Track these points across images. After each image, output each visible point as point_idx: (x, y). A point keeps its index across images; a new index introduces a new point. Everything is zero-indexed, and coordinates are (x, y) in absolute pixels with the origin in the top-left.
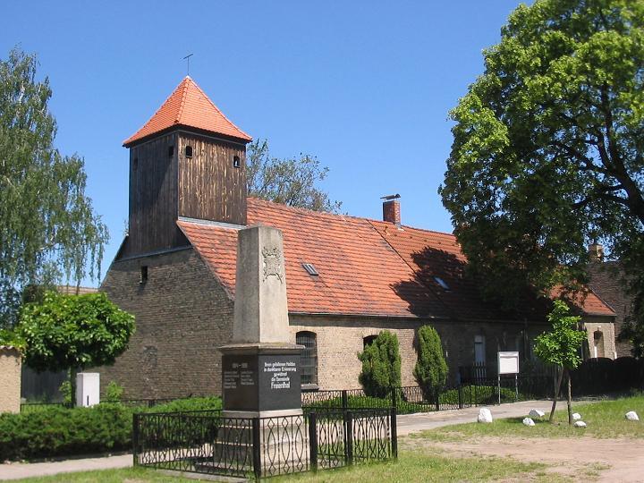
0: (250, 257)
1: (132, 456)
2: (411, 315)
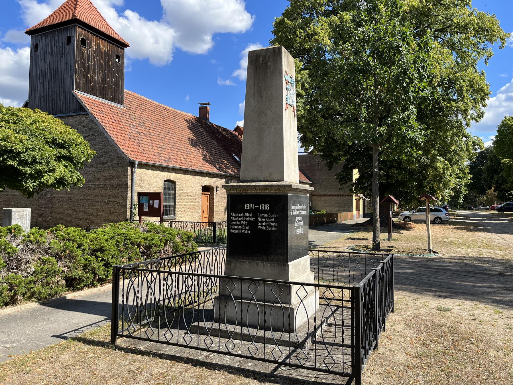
2: (307, 187)
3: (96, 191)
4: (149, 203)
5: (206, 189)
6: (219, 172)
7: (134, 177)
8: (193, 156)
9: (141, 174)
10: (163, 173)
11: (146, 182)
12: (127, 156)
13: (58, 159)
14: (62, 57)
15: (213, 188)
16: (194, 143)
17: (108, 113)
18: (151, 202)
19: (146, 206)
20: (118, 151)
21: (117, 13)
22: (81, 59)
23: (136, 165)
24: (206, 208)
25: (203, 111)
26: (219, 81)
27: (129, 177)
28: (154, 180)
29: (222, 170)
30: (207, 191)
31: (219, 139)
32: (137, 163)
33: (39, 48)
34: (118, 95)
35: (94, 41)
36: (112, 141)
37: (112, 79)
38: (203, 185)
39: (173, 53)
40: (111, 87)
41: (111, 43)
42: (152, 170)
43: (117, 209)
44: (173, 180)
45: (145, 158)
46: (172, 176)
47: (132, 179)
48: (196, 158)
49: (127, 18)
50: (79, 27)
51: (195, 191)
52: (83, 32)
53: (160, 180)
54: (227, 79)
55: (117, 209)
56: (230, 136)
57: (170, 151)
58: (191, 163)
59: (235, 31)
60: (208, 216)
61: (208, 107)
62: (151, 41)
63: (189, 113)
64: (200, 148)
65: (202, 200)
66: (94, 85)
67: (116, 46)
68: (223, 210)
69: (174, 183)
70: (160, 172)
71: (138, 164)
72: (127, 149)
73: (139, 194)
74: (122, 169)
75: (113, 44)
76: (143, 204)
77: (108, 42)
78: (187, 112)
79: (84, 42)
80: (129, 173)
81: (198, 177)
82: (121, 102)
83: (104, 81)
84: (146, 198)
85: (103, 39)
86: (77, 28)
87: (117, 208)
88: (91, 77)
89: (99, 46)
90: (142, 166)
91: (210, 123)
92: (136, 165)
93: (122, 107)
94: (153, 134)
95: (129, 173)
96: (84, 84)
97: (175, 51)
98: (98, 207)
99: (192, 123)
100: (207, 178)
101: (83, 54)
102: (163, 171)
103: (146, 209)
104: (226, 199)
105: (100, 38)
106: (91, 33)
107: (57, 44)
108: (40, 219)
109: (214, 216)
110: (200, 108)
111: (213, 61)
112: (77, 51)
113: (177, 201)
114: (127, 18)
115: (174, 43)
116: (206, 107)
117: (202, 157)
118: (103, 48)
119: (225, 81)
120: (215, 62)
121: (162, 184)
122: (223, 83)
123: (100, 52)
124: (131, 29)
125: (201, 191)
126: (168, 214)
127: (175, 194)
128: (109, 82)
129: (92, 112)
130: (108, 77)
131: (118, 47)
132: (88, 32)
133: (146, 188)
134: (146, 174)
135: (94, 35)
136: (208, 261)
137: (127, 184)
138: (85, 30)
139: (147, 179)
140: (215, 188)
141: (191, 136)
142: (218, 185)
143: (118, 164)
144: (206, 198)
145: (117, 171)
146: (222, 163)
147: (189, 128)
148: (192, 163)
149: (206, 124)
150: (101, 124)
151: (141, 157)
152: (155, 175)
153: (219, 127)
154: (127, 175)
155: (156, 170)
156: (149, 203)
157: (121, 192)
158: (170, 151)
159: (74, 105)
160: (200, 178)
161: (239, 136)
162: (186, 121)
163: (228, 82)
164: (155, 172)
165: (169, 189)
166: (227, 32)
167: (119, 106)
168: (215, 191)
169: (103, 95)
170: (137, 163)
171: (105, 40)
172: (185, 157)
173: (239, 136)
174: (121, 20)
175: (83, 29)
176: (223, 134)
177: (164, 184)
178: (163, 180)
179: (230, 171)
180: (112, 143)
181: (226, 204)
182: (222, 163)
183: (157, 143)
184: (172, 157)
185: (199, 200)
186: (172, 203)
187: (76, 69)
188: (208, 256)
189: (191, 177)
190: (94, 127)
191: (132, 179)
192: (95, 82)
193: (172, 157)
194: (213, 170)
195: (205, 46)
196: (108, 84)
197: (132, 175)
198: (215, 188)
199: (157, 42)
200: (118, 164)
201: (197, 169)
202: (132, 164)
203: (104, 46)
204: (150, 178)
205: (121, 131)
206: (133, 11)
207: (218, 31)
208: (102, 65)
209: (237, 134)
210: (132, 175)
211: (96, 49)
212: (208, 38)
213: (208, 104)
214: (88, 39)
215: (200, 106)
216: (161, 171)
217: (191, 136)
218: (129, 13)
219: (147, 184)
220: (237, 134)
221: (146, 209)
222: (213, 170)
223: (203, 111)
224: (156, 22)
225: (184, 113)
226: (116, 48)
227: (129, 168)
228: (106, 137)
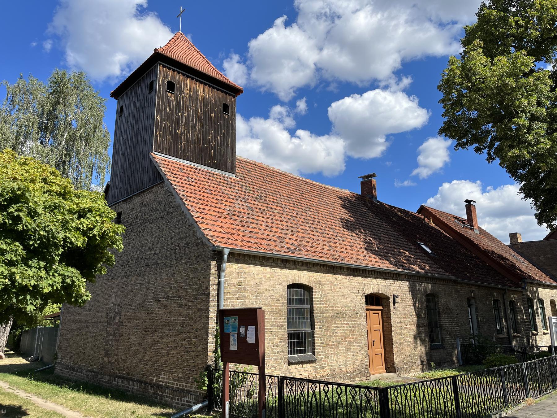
0: (288, 265)
3: (168, 310)
4: (239, 333)
5: (374, 300)
6: (396, 269)
7: (222, 280)
8: (347, 244)
9: (239, 273)
10: (284, 271)
11: (249, 288)
12: (209, 240)
14: (143, 112)
15: (387, 298)
16: (348, 226)
17: (201, 181)
18: (242, 330)
19: (234, 340)
20: (198, 234)
21: (290, 134)
22: (166, 108)
23: (226, 257)
24: (378, 337)
25: (367, 185)
26: (395, 184)
27: (213, 280)
28: (266, 285)
29: (400, 266)
30: (378, 305)
31: (394, 221)
32: (227, 251)
33: (124, 109)
34: (227, 159)
35: (188, 85)
36: (190, 217)
37: (215, 137)
38: (368, 293)
39: (346, 162)
40: (214, 148)
41: (214, 88)
42: (261, 265)
43: (194, 345)
44: (306, 283)
45: (250, 244)
46: (303, 277)
47: (219, 284)
48: (353, 248)
49: (299, 137)
50: (164, 66)
51: (353, 305)
52: (171, 73)
53: (280, 284)
54: (405, 180)
55: (194, 345)
56: (412, 219)
57: (304, 235)
58: (341, 254)
59: (408, 129)
60: (382, 351)
61: (374, 180)
62: (323, 154)
63: (345, 189)
64: (362, 232)
65: (367, 322)
66: (187, 146)
67: (222, 91)
68: (411, 339)
69: (308, 289)
70: (278, 270)
71: (230, 254)
72: (214, 229)
73: (222, 314)
74: (203, 265)
75: (218, 90)
76: (228, 335)
77: (210, 86)
78: (340, 188)
79: (171, 86)
80: (213, 272)
81: (356, 278)
82: (232, 170)
83: (203, 139)
84: (232, 321)
85: (201, 83)
86: (160, 68)
87: (194, 341)
88: (181, 134)
89: (196, 92)
90: (239, 257)
91: (378, 202)
92: (226, 257)
93: (233, 177)
94: (276, 211)
95: (213, 272)
96: (171, 143)
97: (347, 159)
98: (169, 341)
99: (350, 201)
100: (374, 280)
101: (169, 102)
102: (285, 267)
103: (234, 347)
104: (415, 318)
105: (197, 81)
106: (183, 75)
107: (139, 98)
108: (106, 359)
109: (395, 351)
110: (362, 183)
111: (388, 163)
112: (159, 97)
113: (317, 325)
114: (299, 137)
115: (345, 152)
116: (371, 181)
117: (363, 245)
118: (201, 95)
119: (403, 182)
120: (391, 163)
121: (284, 292)
122: (400, 185)
123: (197, 99)
124: (304, 147)
125: (364, 305)
126: (299, 352)
127: (311, 311)
128: (210, 142)
129: (169, 178)
130: (209, 134)
131: (226, 93)
132: (179, 73)
133: (249, 300)
134: (249, 274)
135: (188, 77)
136: (406, 399)
137: (209, 294)
138: (174, 71)
139: (252, 282)
140: (391, 299)
141: (347, 217)
142: (396, 293)
143: (197, 257)
144: (376, 318)
145: (196, 270)
146: (401, 254)
147: (344, 206)
148: (344, 255)
149: (373, 203)
150: (177, 193)
151: (240, 243)
152: (268, 276)
153: (394, 207)
154: (208, 276)
155: (271, 266)
156: (239, 333)
157: (201, 309)
158: (304, 235)
159: (151, 175)
160: (361, 279)
161: (426, 220)
162: (340, 198)
163: (406, 183)
164: (268, 269)
165: (301, 301)
166: (401, 132)
167: (227, 174)
168: (392, 304)
169: (201, 158)
170: (227, 251)
171: (206, 84)
172: (332, 244)
173: (426, 220)
174: (295, 140)
175: (169, 69)
176: (399, 217)
177: (289, 293)
178: (285, 285)
179: (416, 268)
180: (191, 220)
181: (414, 327)
182: (401, 254)
183: (282, 223)
184: (306, 244)
185: (362, 321)
186: (308, 329)
187: (157, 123)
188: (406, 392)
189: (341, 279)
190: (170, 200)
191: (219, 284)
192: (188, 141)
193: (306, 244)
195: (378, 149)
196: (209, 143)
197: (219, 276)
198: (391, 299)
199: (329, 154)
200: (197, 257)
201: (353, 263)
202: (218, 255)
203: (204, 91)
204: (258, 281)
205: (217, 205)
206: (304, 129)
207: (389, 132)
208: (200, 118)
209: (423, 217)
210: (219, 276)
211: (190, 95)
212: (382, 140)
213: (373, 176)
214: (178, 81)
215: (362, 180)
216: (280, 267)
217: (347, 217)
218: (300, 132)
219: (252, 292)
220: (423, 217)
221: (234, 347)
222: (386, 265)
223: (367, 185)
224: (326, 136)
225: (337, 189)
226: (221, 95)
227: (213, 263)
228: (183, 212)
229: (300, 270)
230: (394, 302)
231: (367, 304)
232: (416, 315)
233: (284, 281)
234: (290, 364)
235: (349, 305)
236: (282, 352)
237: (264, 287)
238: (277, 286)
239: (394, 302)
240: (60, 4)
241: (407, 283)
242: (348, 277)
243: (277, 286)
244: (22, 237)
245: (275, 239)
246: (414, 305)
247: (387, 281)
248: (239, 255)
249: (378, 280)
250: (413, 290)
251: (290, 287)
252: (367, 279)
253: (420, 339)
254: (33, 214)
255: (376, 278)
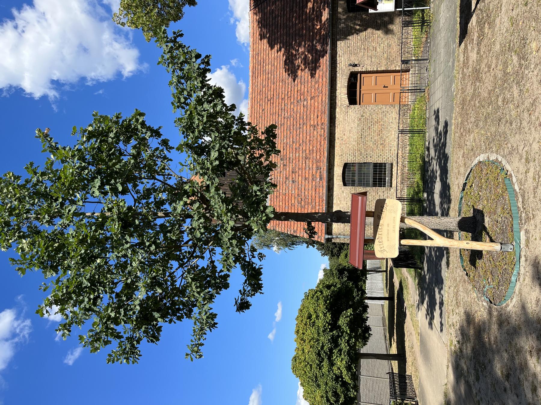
1: (362, 360)
6: (327, 57)
13: (332, 364)
23: (330, 237)
32: (327, 236)
38: (347, 102)
46: (338, 171)
51: (356, 120)
53: (343, 192)
69: (346, 166)
81: (337, 115)
92: (330, 237)
104: (370, 30)
113: (369, 160)
152: (339, 202)
160: (337, 110)
164: (335, 201)
170: (327, 236)
186: (371, 167)
194: (325, 61)
216: (333, 192)
222: (325, 61)
229: (333, 175)
230: (355, 65)
231: (356, 104)
232: (365, 30)
233: (341, 188)
234: (391, 186)
235: (356, 125)
236: (383, 192)
237: (345, 205)
238: (345, 195)
239: (355, 65)
240: (31, 4)
241: (338, 43)
242: (336, 125)
243: (345, 195)
244: (331, 350)
245: (314, 183)
246: (358, 32)
247: (338, 75)
248: (330, 126)
249: (338, 88)
250: (346, 33)
251: (345, 184)
252: (337, 101)
253: (388, 24)
254: (322, 347)
255: (336, 90)
